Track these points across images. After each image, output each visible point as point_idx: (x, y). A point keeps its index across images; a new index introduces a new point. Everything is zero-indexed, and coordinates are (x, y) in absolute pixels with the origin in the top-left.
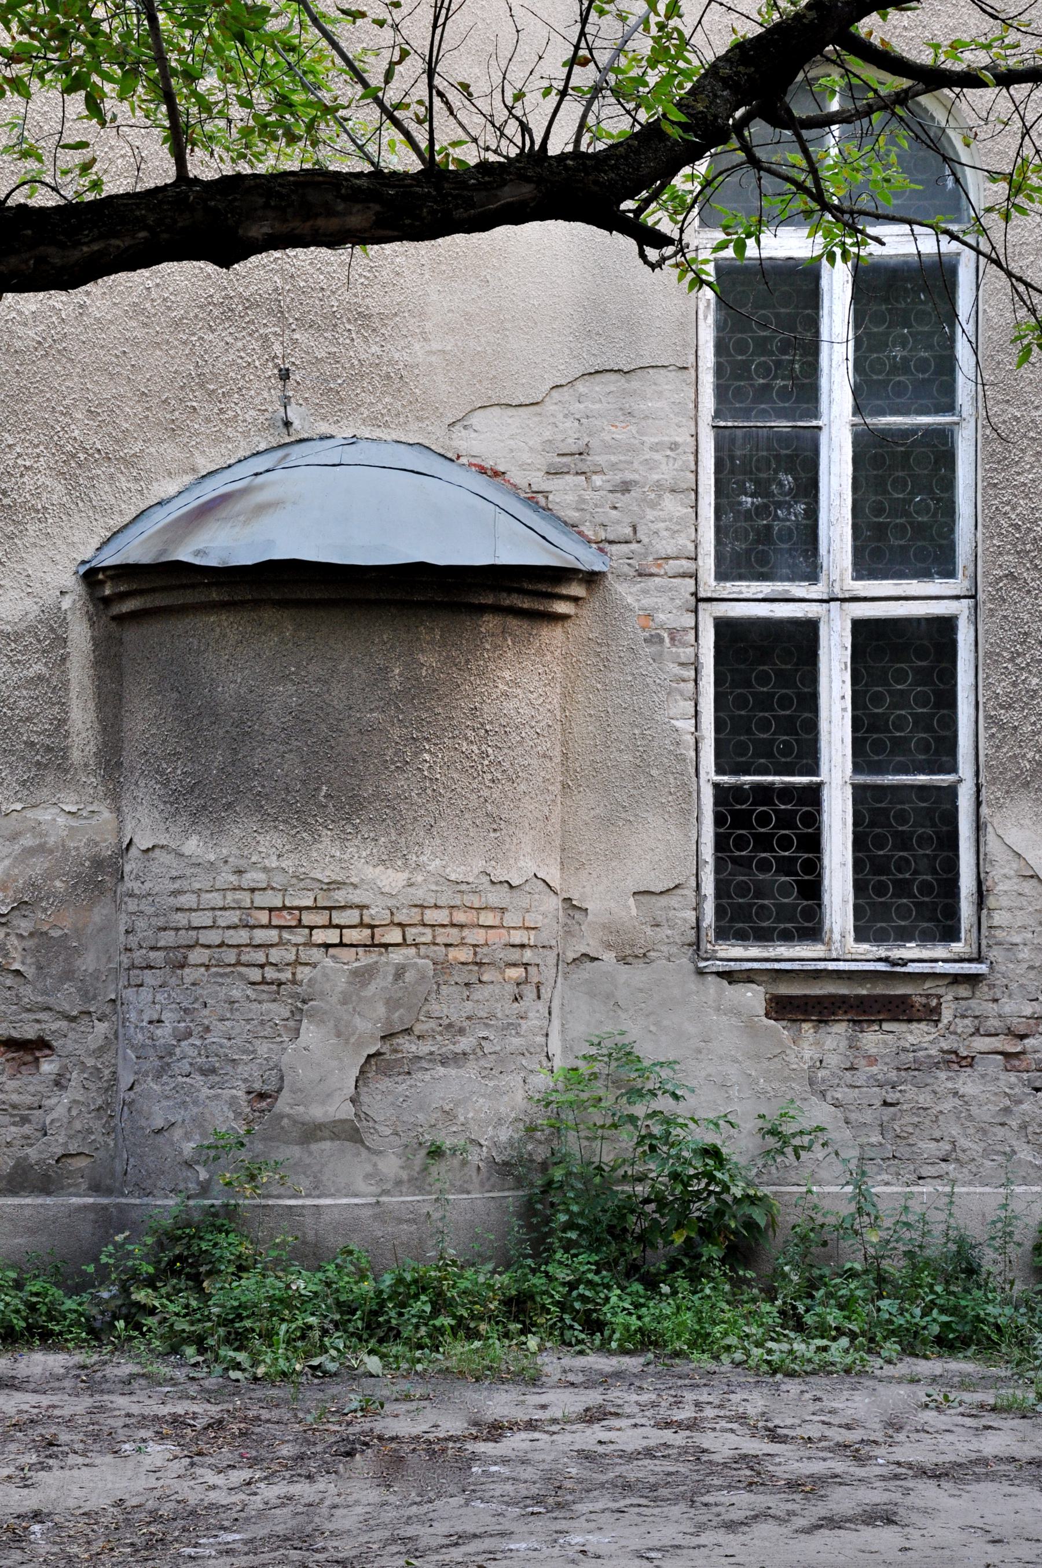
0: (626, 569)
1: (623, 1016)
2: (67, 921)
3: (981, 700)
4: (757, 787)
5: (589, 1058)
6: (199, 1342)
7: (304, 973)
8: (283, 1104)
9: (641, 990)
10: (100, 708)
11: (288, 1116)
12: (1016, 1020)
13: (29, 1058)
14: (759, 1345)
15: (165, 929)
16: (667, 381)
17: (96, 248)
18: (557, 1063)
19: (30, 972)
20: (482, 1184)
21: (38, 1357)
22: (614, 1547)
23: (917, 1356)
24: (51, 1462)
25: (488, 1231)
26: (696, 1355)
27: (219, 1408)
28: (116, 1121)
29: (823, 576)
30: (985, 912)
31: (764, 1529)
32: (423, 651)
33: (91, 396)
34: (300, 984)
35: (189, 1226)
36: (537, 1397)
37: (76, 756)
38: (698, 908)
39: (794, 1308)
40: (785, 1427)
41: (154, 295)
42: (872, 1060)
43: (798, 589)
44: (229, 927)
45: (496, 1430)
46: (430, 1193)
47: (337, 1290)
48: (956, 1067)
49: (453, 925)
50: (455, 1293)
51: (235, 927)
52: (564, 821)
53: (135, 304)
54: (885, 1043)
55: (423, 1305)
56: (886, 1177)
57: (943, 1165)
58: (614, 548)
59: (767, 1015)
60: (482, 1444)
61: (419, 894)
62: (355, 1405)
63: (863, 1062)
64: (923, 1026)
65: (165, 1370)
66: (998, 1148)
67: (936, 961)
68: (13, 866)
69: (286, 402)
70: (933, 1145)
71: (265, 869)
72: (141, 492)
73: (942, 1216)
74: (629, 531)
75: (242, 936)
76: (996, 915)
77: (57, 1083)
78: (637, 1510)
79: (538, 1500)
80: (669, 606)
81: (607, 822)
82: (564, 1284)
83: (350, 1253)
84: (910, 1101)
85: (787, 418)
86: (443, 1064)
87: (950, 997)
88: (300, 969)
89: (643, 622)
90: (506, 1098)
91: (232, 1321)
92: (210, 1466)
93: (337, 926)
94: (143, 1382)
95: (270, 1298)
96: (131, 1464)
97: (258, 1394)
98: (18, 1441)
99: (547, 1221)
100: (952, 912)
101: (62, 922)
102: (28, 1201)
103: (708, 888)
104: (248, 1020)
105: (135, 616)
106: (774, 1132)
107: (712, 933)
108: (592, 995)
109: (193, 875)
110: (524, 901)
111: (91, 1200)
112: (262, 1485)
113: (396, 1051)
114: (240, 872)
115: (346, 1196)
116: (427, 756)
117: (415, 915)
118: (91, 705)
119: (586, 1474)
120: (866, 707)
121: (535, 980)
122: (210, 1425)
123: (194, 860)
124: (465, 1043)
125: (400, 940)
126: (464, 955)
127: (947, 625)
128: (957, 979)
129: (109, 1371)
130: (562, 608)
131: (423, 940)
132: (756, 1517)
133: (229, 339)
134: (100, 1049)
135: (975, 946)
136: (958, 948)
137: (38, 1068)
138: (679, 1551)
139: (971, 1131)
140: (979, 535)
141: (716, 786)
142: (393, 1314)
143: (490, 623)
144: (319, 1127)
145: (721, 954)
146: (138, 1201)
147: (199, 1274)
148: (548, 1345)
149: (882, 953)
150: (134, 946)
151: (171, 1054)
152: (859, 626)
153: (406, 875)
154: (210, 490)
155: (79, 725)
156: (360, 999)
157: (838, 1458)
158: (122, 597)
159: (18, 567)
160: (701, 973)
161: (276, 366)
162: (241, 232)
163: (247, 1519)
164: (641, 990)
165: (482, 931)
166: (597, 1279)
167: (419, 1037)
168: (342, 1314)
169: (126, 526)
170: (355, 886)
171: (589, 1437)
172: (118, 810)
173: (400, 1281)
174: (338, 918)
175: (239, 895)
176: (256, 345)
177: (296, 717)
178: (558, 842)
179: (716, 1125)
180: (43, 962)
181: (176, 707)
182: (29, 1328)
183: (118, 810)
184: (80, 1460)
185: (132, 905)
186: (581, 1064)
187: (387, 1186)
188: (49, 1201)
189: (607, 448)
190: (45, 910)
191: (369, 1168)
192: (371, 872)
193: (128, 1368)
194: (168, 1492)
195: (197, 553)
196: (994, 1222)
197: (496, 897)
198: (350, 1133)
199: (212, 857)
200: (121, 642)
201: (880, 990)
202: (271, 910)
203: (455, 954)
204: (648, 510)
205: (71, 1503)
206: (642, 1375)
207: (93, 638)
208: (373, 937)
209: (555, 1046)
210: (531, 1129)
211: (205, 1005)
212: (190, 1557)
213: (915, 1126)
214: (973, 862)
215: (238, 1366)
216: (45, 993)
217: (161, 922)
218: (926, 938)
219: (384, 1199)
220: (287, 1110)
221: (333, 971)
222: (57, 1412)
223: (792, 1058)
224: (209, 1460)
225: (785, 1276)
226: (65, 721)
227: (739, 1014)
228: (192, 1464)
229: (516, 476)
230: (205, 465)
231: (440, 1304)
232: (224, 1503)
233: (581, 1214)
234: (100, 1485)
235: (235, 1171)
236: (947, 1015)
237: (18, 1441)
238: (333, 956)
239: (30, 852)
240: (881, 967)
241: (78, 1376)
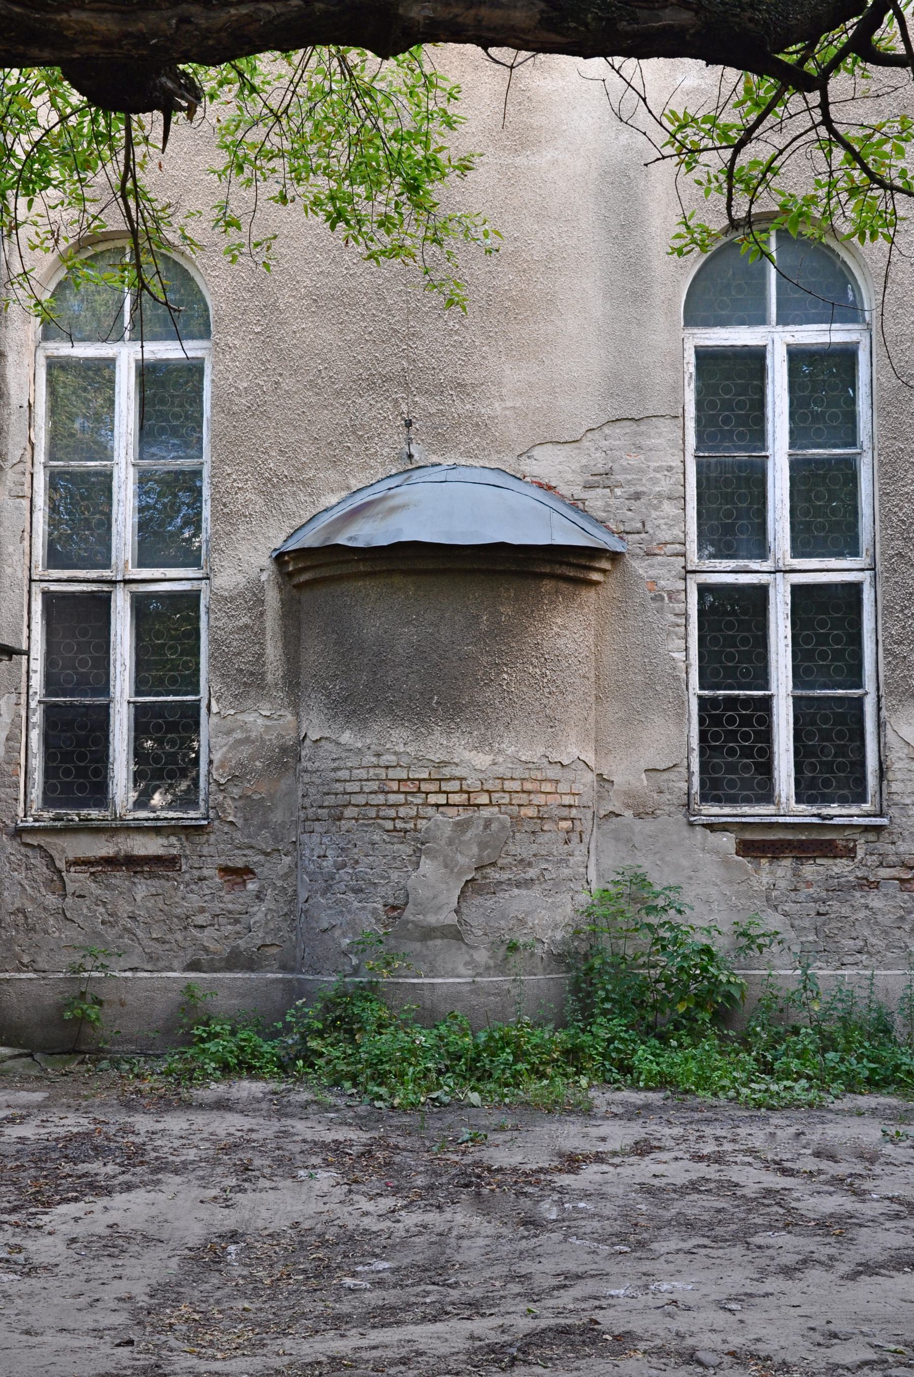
0: (638, 551)
1: (639, 854)
2: (264, 790)
3: (880, 639)
4: (728, 698)
5: (616, 883)
6: (353, 1078)
7: (422, 824)
8: (408, 914)
9: (650, 836)
10: (285, 646)
11: (412, 922)
12: (907, 857)
13: (240, 880)
14: (744, 1085)
15: (328, 794)
16: (665, 426)
17: (244, 12)
18: (594, 886)
19: (240, 823)
20: (545, 970)
21: (245, 1084)
22: (697, 1295)
23: (855, 1093)
24: (246, 1185)
25: (549, 1001)
26: (700, 1093)
27: (368, 1135)
28: (297, 923)
29: (771, 556)
30: (885, 782)
31: (815, 1274)
32: (502, 604)
33: (281, 441)
34: (420, 831)
35: (346, 995)
36: (595, 1129)
37: (270, 678)
38: (689, 781)
39: (764, 1057)
40: (787, 1160)
41: (323, 375)
42: (809, 884)
43: (754, 565)
44: (371, 793)
45: (572, 1162)
46: (509, 975)
47: (447, 1044)
48: (867, 889)
49: (523, 792)
50: (529, 1046)
51: (375, 793)
52: (597, 722)
53: (311, 381)
54: (818, 872)
55: (507, 1055)
56: (819, 964)
57: (858, 955)
58: (630, 537)
59: (737, 854)
60: (565, 1176)
61: (501, 770)
62: (467, 1137)
63: (803, 885)
64: (844, 861)
65: (331, 1099)
66: (896, 944)
67: (852, 816)
68: (228, 751)
69: (409, 442)
70: (851, 942)
72: (313, 503)
73: (865, 993)
74: (639, 525)
76: (893, 784)
77: (258, 897)
78: (703, 1251)
79: (622, 1237)
80: (668, 576)
81: (627, 722)
82: (603, 1040)
83: (456, 1017)
84: (836, 912)
85: (746, 450)
86: (517, 887)
87: (862, 841)
88: (419, 821)
89: (650, 586)
90: (560, 910)
91: (376, 1064)
92: (364, 1194)
93: (445, 792)
94: (315, 1107)
95: (402, 1049)
96: (305, 1189)
97: (395, 1122)
98: (225, 1164)
99: (589, 995)
100: (862, 781)
101: (260, 789)
102: (239, 975)
103: (695, 767)
104: (384, 856)
105: (306, 584)
106: (744, 934)
107: (698, 798)
108: (617, 839)
109: (347, 757)
110: (571, 775)
111: (280, 976)
112: (403, 1213)
113: (486, 878)
114: (378, 755)
115: (452, 977)
116: (505, 676)
117: (498, 785)
118: (280, 644)
119: (655, 1211)
120: (799, 645)
121: (579, 829)
122: (363, 1154)
123: (347, 747)
124: (532, 873)
125: (487, 802)
126: (531, 812)
127: (855, 588)
128: (867, 829)
129: (293, 1097)
130: (595, 576)
131: (503, 801)
132: (804, 1262)
133: (372, 402)
134: (286, 874)
135: (878, 806)
136: (867, 807)
137: (245, 886)
138: (752, 1300)
139: (878, 932)
140: (877, 527)
141: (700, 697)
142: (487, 1061)
143: (548, 585)
144: (433, 929)
145: (704, 812)
146: (311, 977)
147: (352, 1029)
148: (595, 1083)
149: (816, 812)
150: (308, 805)
151: (333, 879)
152: (797, 590)
153: (492, 757)
154: (359, 500)
155: (272, 658)
156: (461, 842)
157: (841, 1193)
158: (300, 571)
159: (233, 553)
160: (691, 824)
161: (403, 419)
162: (401, 11)
163: (393, 1246)
164: (650, 836)
165: (543, 796)
166: (626, 1036)
167: (501, 869)
168: (452, 1060)
169: (303, 526)
170: (457, 765)
171: (644, 1169)
172: (297, 714)
173: (491, 1037)
174: (445, 787)
175: (378, 771)
176: (389, 405)
177: (416, 649)
178: (593, 736)
179: (709, 932)
180: (248, 816)
181: (335, 644)
182: (240, 1063)
183: (297, 714)
184: (268, 1184)
185: (306, 778)
186: (609, 886)
187: (481, 970)
188: (253, 975)
189: (625, 470)
190: (249, 781)
191: (467, 958)
192: (468, 755)
193: (306, 1096)
194: (333, 1217)
195: (350, 539)
196: (902, 998)
197: (553, 772)
198: (455, 934)
199: (360, 745)
200: (299, 602)
201: (814, 836)
202: (399, 781)
203: (525, 811)
204: (653, 512)
205: (260, 1224)
206: (664, 1108)
207: (281, 600)
208: (469, 799)
209: (592, 875)
210: (577, 932)
211: (355, 845)
212: (350, 1289)
213: (840, 929)
214: (876, 749)
215: (380, 1097)
216: (249, 837)
218: (843, 801)
219: (478, 979)
220: (411, 917)
221: (443, 822)
222: (254, 1136)
223: (754, 883)
224: (363, 1188)
225: (756, 1034)
226: (262, 655)
227: (717, 853)
228: (350, 1191)
229: (564, 490)
230: (355, 484)
231: (520, 1055)
232: (375, 1229)
233: (614, 990)
234: (282, 1206)
235: (377, 959)
236: (860, 853)
237: (225, 1164)
238: (442, 813)
239: (240, 742)
240: (815, 820)
241: (271, 1100)
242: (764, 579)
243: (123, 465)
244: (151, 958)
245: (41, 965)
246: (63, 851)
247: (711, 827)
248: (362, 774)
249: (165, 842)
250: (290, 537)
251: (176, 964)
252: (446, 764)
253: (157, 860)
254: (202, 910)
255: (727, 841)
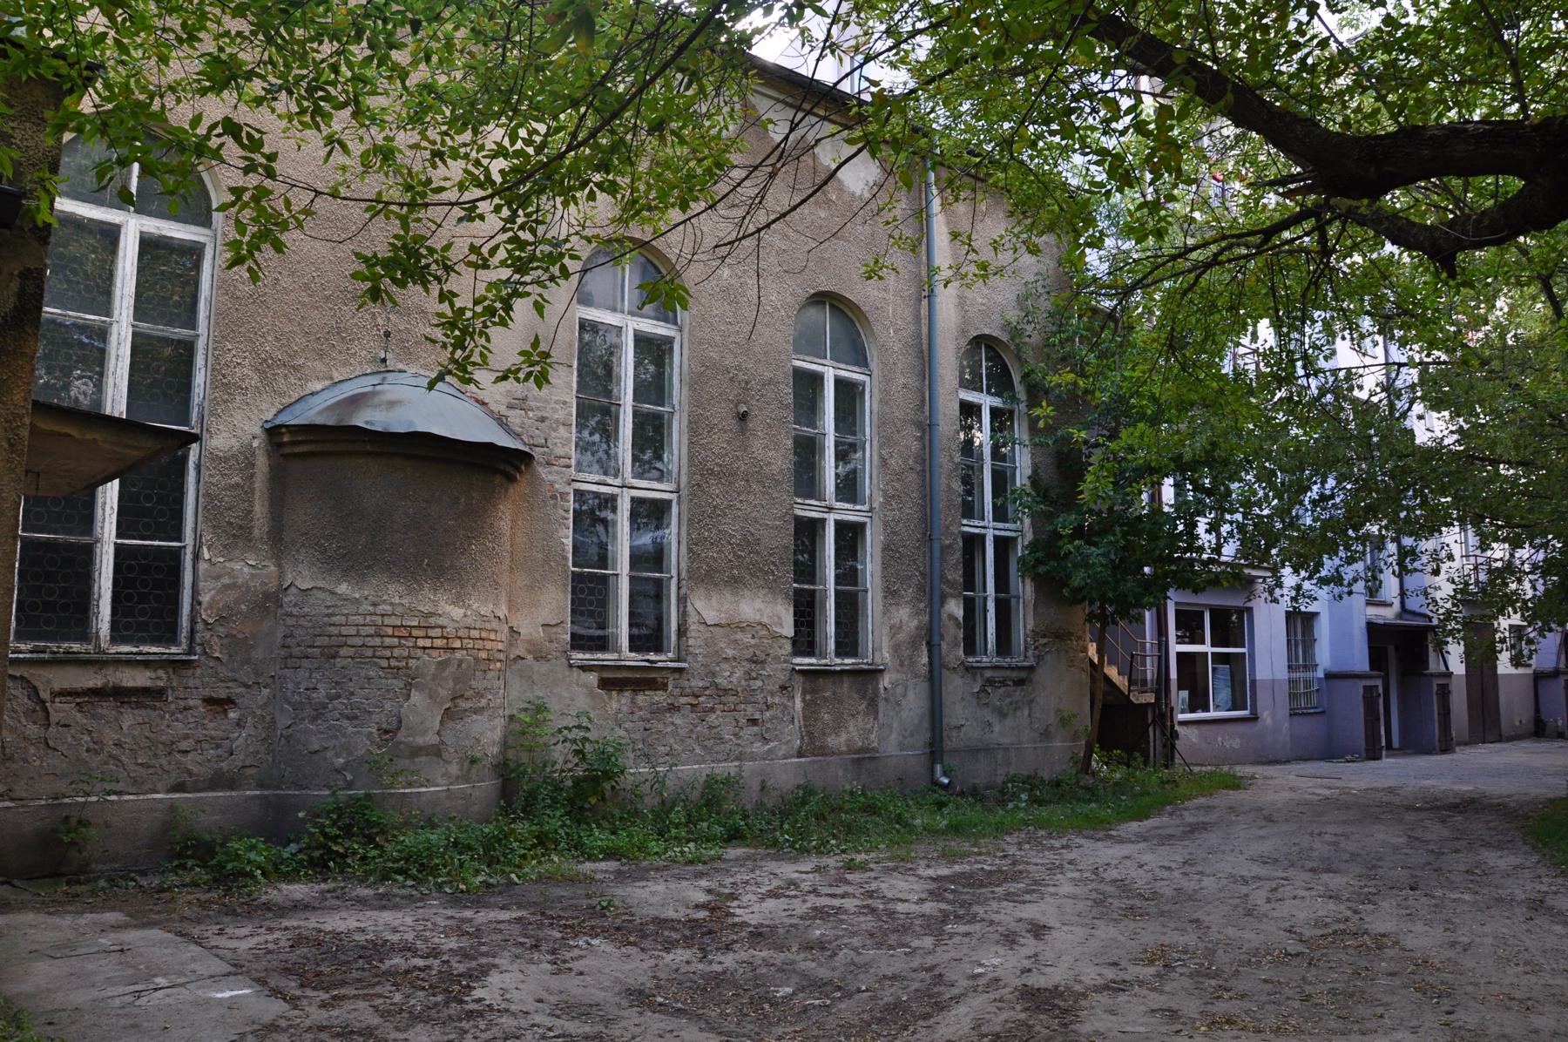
7: (412, 663)
8: (401, 736)
10: (271, 506)
19: (225, 658)
37: (256, 532)
42: (640, 709)
61: (469, 621)
71: (391, 604)
75: (377, 641)
81: (531, 588)
114: (375, 605)
124: (483, 702)
126: (483, 655)
136: (670, 655)
152: (633, 499)
158: (293, 443)
174: (431, 633)
183: (279, 566)
189: (535, 399)
192: (449, 608)
198: (436, 752)
217: (318, 631)
226: (250, 512)
229: (493, 406)
230: (337, 377)
236: (670, 687)
239: (226, 587)
242: (616, 491)
243: (124, 324)
244: (135, 782)
245: (18, 794)
246: (49, 682)
247: (583, 668)
248: (360, 620)
249: (153, 675)
250: (280, 412)
251: (159, 786)
252: (432, 614)
253: (145, 691)
254: (187, 737)
255: (592, 678)
